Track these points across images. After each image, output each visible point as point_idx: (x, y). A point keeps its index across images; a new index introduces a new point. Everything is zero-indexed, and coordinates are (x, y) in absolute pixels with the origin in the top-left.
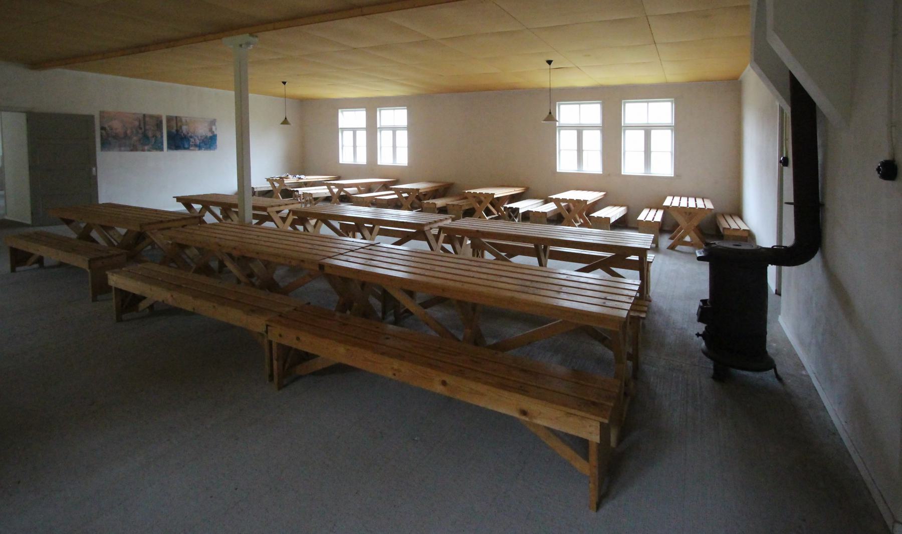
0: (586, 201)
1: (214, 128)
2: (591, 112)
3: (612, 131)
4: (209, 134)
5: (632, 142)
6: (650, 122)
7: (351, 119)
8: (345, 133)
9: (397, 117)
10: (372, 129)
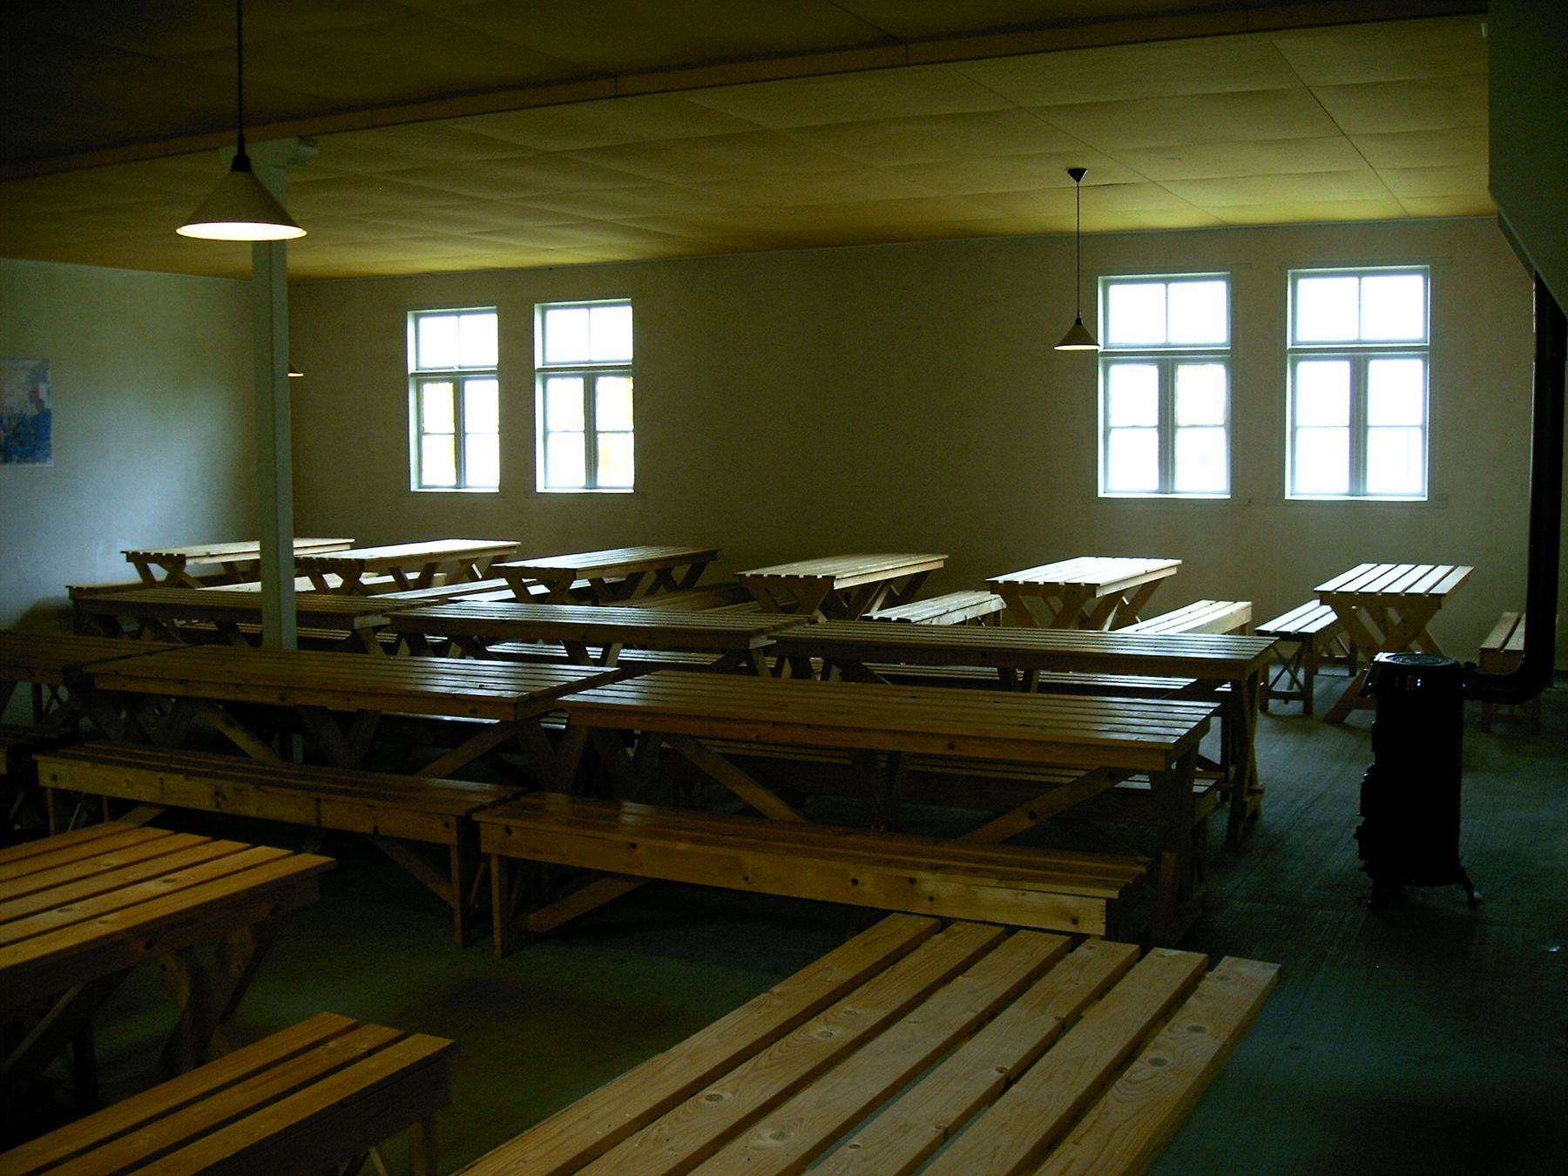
0: (1092, 588)
1: (43, 387)
2: (1198, 309)
3: (1259, 363)
4: (31, 411)
5: (1316, 395)
6: (1173, 340)
7: (452, 340)
8: (429, 389)
9: (594, 332)
10: (518, 375)
